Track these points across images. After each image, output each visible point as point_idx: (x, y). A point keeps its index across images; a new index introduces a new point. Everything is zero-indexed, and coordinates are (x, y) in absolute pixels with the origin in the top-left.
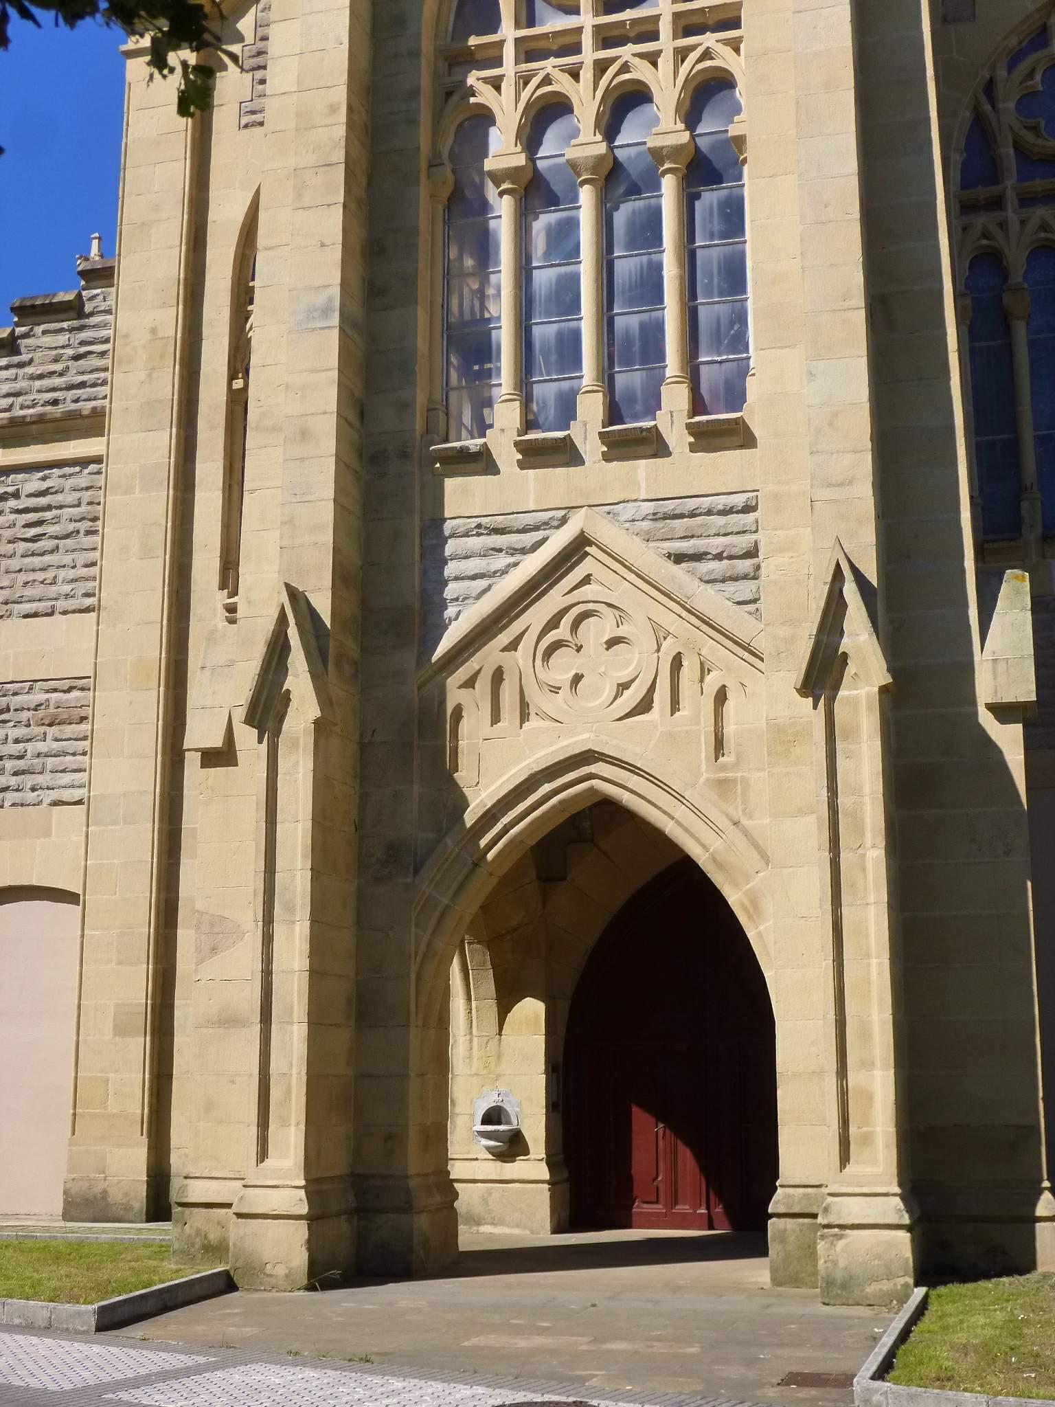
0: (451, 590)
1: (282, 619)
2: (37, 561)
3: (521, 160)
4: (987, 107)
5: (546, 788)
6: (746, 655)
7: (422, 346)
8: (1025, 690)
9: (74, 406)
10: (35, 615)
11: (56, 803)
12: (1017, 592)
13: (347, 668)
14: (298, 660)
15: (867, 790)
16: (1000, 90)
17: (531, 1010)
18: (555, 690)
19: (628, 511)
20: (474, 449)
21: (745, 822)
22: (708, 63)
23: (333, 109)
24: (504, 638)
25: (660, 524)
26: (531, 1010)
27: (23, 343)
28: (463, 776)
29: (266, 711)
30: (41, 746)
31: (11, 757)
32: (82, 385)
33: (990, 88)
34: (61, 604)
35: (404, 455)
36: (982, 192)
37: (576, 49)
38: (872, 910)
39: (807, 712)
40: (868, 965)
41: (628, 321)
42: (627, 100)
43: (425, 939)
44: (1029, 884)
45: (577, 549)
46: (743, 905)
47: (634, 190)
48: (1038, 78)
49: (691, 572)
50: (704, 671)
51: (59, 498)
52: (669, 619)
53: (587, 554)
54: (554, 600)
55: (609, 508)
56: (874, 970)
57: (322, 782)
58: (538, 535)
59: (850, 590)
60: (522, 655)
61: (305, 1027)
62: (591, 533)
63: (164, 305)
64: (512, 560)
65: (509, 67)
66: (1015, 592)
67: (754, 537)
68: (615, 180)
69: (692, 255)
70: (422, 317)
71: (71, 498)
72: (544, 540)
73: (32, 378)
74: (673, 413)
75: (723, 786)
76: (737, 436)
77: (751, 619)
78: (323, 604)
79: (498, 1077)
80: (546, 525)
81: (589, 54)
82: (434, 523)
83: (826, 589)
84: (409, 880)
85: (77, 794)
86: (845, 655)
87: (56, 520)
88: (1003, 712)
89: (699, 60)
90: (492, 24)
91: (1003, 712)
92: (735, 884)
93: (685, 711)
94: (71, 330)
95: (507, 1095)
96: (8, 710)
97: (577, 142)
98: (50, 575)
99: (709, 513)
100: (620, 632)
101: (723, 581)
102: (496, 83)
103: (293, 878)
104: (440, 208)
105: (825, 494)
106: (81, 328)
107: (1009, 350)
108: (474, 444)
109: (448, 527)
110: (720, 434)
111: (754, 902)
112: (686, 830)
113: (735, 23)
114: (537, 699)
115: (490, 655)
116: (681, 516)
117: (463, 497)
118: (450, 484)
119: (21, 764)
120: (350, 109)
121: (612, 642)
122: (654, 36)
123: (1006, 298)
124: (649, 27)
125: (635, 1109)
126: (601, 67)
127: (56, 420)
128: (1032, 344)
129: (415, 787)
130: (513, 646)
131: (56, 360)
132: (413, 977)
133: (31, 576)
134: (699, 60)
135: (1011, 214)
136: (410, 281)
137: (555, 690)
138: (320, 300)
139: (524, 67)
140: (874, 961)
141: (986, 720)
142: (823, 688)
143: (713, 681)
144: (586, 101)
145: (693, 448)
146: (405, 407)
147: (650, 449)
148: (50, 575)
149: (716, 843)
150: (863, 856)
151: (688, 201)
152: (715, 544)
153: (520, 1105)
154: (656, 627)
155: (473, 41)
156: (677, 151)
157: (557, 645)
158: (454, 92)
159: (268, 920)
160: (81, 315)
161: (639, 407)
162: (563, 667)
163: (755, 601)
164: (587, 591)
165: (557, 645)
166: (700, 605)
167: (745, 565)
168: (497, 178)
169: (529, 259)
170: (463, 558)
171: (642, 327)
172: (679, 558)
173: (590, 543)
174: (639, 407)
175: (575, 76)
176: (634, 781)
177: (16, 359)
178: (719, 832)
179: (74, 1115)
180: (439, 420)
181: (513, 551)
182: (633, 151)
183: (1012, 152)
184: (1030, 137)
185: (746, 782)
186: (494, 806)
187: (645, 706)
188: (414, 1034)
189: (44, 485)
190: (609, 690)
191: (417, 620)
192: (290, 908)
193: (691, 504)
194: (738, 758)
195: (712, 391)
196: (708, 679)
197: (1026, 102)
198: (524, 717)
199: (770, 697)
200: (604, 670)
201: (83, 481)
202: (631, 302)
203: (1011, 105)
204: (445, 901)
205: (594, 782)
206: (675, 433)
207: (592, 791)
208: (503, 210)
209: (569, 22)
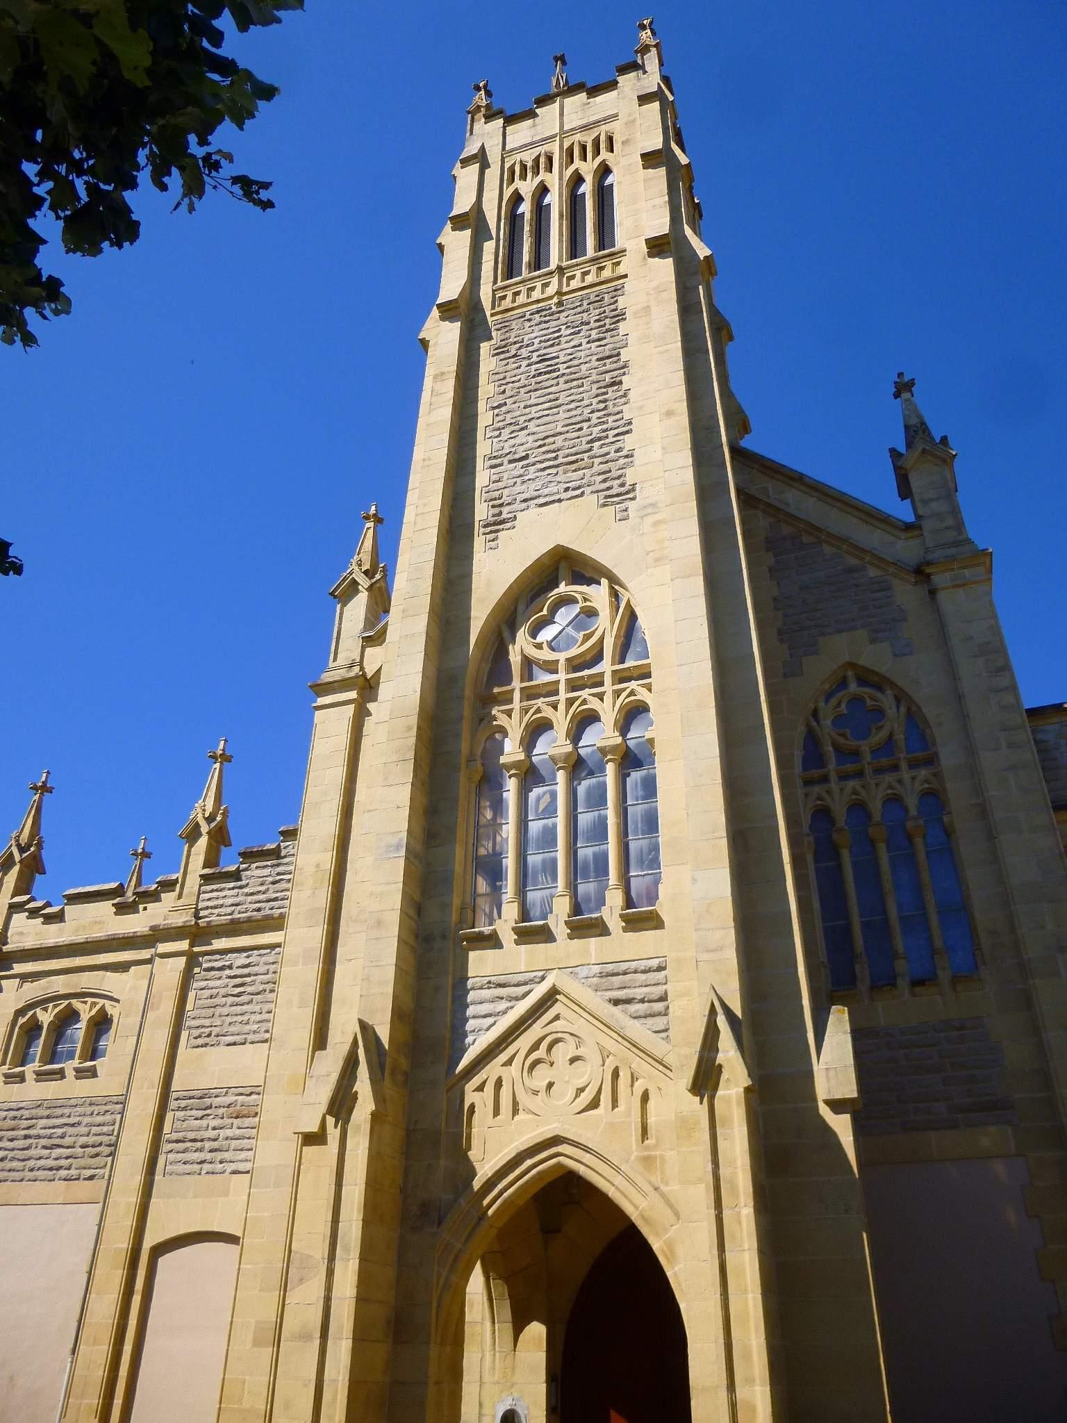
0: (470, 1025)
1: (355, 1043)
2: (238, 1009)
3: (522, 756)
4: (814, 724)
5: (529, 1162)
6: (661, 1068)
7: (458, 869)
8: (849, 1090)
9: (269, 912)
10: (234, 1044)
11: (234, 1172)
12: (840, 1021)
13: (400, 1078)
14: (363, 1071)
15: (739, 1163)
16: (821, 715)
17: (536, 1331)
18: (536, 1093)
19: (583, 972)
20: (487, 933)
21: (663, 1188)
22: (632, 698)
23: (409, 728)
24: (503, 1057)
25: (603, 980)
26: (536, 1331)
27: (244, 874)
28: (473, 1155)
29: (341, 1106)
30: (229, 1133)
31: (209, 1139)
32: (275, 899)
33: (815, 713)
34: (251, 1037)
35: (444, 937)
36: (815, 773)
37: (556, 693)
38: (746, 1255)
39: (695, 1107)
40: (746, 1300)
41: (586, 852)
42: (588, 719)
43: (444, 1274)
44: (865, 1235)
45: (551, 997)
46: (662, 1251)
47: (591, 773)
48: (843, 706)
49: (625, 1012)
50: (634, 1079)
51: (255, 969)
52: (610, 1044)
53: (557, 1000)
54: (536, 1031)
55: (572, 970)
56: (751, 1303)
57: (375, 1157)
58: (526, 988)
59: (721, 1021)
60: (515, 1068)
61: (350, 1341)
62: (560, 986)
63: (325, 850)
64: (510, 1004)
65: (516, 704)
66: (839, 1024)
67: (665, 987)
68: (577, 767)
69: (625, 810)
70: (459, 851)
71: (262, 969)
72: (530, 991)
73: (247, 895)
74: (612, 909)
75: (648, 1161)
76: (653, 921)
77: (664, 1042)
78: (384, 1033)
79: (512, 1386)
80: (531, 981)
81: (563, 695)
82: (462, 979)
83: (705, 1019)
84: (435, 1229)
85: (248, 1166)
86: (720, 1066)
87: (253, 983)
88: (837, 1106)
89: (628, 696)
90: (509, 681)
91: (837, 1106)
92: (657, 1234)
93: (622, 1107)
94: (272, 866)
95: (518, 1400)
96: (211, 1107)
97: (553, 745)
98: (245, 1018)
99: (635, 972)
100: (578, 1053)
101: (645, 1017)
102: (509, 713)
103: (351, 1226)
104: (474, 786)
105: (704, 956)
106: (278, 865)
107: (839, 867)
108: (487, 930)
109: (470, 983)
110: (641, 918)
111: (670, 1246)
112: (626, 1196)
113: (648, 675)
114: (522, 1098)
115: (493, 1070)
116: (618, 974)
117: (480, 964)
118: (473, 955)
119: (215, 1145)
120: (419, 728)
121: (573, 1060)
122: (601, 684)
123: (835, 836)
124: (598, 679)
125: (613, 1414)
126: (570, 702)
127: (257, 921)
128: (854, 864)
129: (442, 1162)
130: (509, 1062)
131: (262, 884)
132: (434, 1304)
133: (235, 1018)
134: (628, 696)
135: (834, 785)
136: (452, 830)
137: (536, 1093)
138: (394, 840)
139: (525, 703)
140: (750, 1296)
141: (824, 1111)
142: (706, 1089)
143: (639, 1086)
144: (561, 721)
145: (625, 930)
146: (445, 907)
147: (598, 931)
148: (245, 1018)
149: (643, 1204)
150: (739, 1213)
151: (622, 777)
152: (639, 993)
153: (528, 1408)
154: (602, 1050)
155: (496, 690)
156: (614, 749)
157: (537, 1062)
158: (483, 718)
159: (332, 1258)
160: (279, 857)
161: (592, 905)
162: (542, 1076)
163: (666, 1030)
164: (557, 1025)
165: (537, 1062)
166: (629, 1033)
167: (659, 1006)
168: (508, 767)
169: (526, 815)
170: (478, 1002)
171: (595, 854)
172: (616, 1002)
173: (559, 993)
174: (592, 905)
175: (555, 708)
176: (587, 1158)
177: (239, 883)
178: (645, 1195)
179: (220, 1409)
180: (469, 913)
181: (510, 999)
182: (589, 750)
183: (831, 749)
184: (841, 740)
185: (662, 1157)
186: (493, 1176)
187: (594, 1104)
188: (434, 1351)
189: (248, 961)
190: (571, 1093)
191: (447, 1044)
192: (347, 1249)
193: (624, 966)
194: (657, 1139)
195: (638, 896)
196: (637, 1084)
197: (838, 721)
198: (515, 1111)
199: (674, 1099)
200: (568, 1078)
201: (271, 959)
202: (588, 840)
203: (829, 722)
204: (459, 1246)
205: (561, 1159)
206: (614, 922)
207: (559, 1165)
208: (511, 787)
209: (553, 677)
